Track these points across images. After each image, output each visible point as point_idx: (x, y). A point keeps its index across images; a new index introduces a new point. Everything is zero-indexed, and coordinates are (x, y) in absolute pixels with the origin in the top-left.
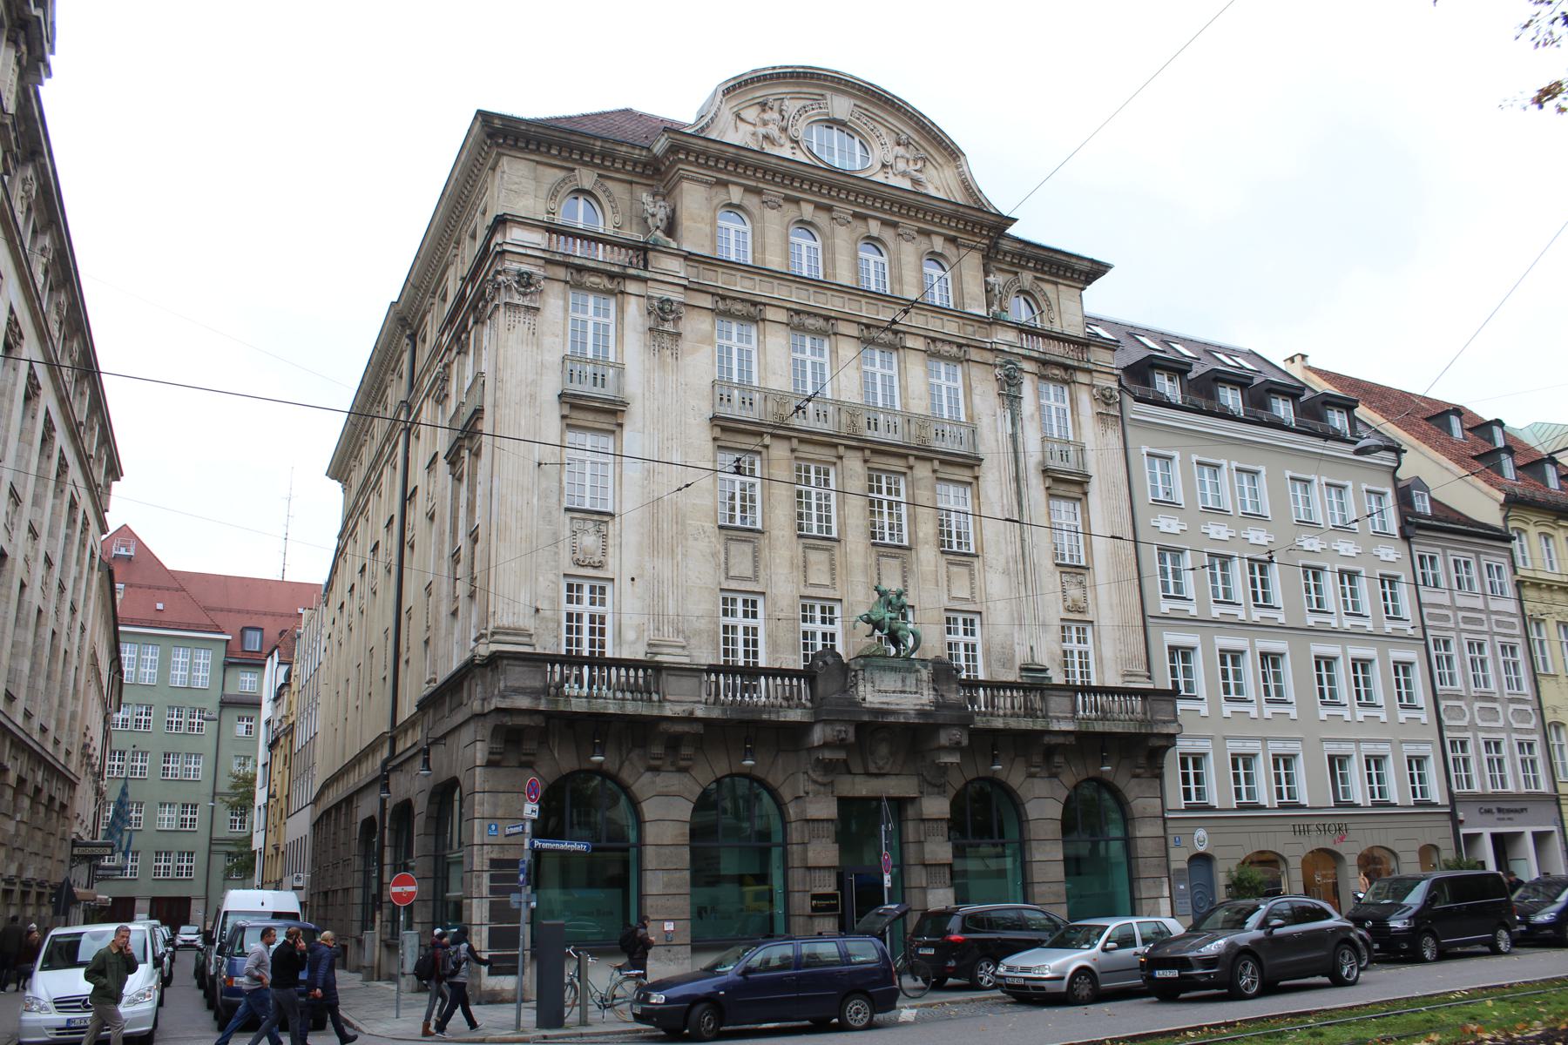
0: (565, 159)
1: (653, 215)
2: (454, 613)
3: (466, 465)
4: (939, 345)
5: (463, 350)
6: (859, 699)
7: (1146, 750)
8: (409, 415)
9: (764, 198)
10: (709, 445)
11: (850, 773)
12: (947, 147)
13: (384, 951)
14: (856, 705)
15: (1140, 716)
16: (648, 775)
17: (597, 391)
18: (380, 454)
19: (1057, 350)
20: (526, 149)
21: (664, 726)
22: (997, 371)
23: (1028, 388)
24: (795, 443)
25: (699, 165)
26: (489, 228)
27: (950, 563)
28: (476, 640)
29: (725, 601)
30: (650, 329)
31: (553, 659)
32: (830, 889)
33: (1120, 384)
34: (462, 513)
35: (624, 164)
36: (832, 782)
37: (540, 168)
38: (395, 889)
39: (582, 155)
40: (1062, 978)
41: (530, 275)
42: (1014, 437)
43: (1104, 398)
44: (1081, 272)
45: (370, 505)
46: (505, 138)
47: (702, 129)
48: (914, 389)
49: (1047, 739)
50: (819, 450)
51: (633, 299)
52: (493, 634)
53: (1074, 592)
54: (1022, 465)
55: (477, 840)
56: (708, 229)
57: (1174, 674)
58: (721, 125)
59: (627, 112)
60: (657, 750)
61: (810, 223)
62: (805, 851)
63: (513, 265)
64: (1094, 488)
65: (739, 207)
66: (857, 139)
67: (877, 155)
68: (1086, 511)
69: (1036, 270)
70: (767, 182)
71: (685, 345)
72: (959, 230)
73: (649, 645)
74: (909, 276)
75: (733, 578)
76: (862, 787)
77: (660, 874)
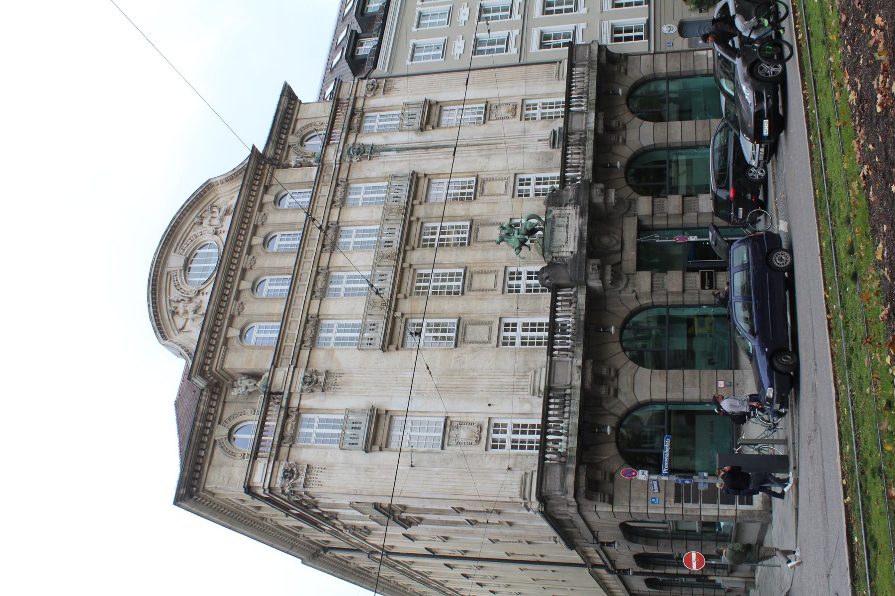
0: (208, 447)
1: (247, 388)
2: (510, 524)
3: (412, 515)
4: (336, 199)
5: (335, 516)
7: (609, 65)
8: (377, 553)
9: (236, 313)
10: (401, 353)
11: (620, 263)
12: (204, 191)
13: (734, 574)
14: (575, 258)
15: (586, 69)
16: (620, 396)
17: (364, 427)
18: (403, 572)
19: (341, 120)
20: (200, 472)
22: (354, 160)
23: (366, 140)
25: (214, 356)
28: (528, 510)
29: (505, 344)
31: (542, 459)
34: (443, 518)
35: (212, 407)
36: (627, 275)
37: (213, 463)
38: (694, 566)
39: (205, 435)
41: (285, 471)
42: (399, 150)
44: (289, 103)
46: (193, 486)
47: (189, 354)
48: (366, 216)
49: (601, 131)
51: (303, 402)
52: (524, 498)
53: (503, 111)
54: (417, 145)
55: (662, 511)
56: (257, 352)
59: (177, 404)
60: (603, 390)
62: (673, 293)
63: (278, 482)
64: (433, 97)
65: (242, 330)
66: (198, 251)
67: (208, 238)
68: (448, 103)
69: (287, 134)
70: (226, 312)
71: (333, 368)
72: (260, 184)
73: (533, 395)
74: (290, 218)
76: (630, 255)
77: (686, 390)
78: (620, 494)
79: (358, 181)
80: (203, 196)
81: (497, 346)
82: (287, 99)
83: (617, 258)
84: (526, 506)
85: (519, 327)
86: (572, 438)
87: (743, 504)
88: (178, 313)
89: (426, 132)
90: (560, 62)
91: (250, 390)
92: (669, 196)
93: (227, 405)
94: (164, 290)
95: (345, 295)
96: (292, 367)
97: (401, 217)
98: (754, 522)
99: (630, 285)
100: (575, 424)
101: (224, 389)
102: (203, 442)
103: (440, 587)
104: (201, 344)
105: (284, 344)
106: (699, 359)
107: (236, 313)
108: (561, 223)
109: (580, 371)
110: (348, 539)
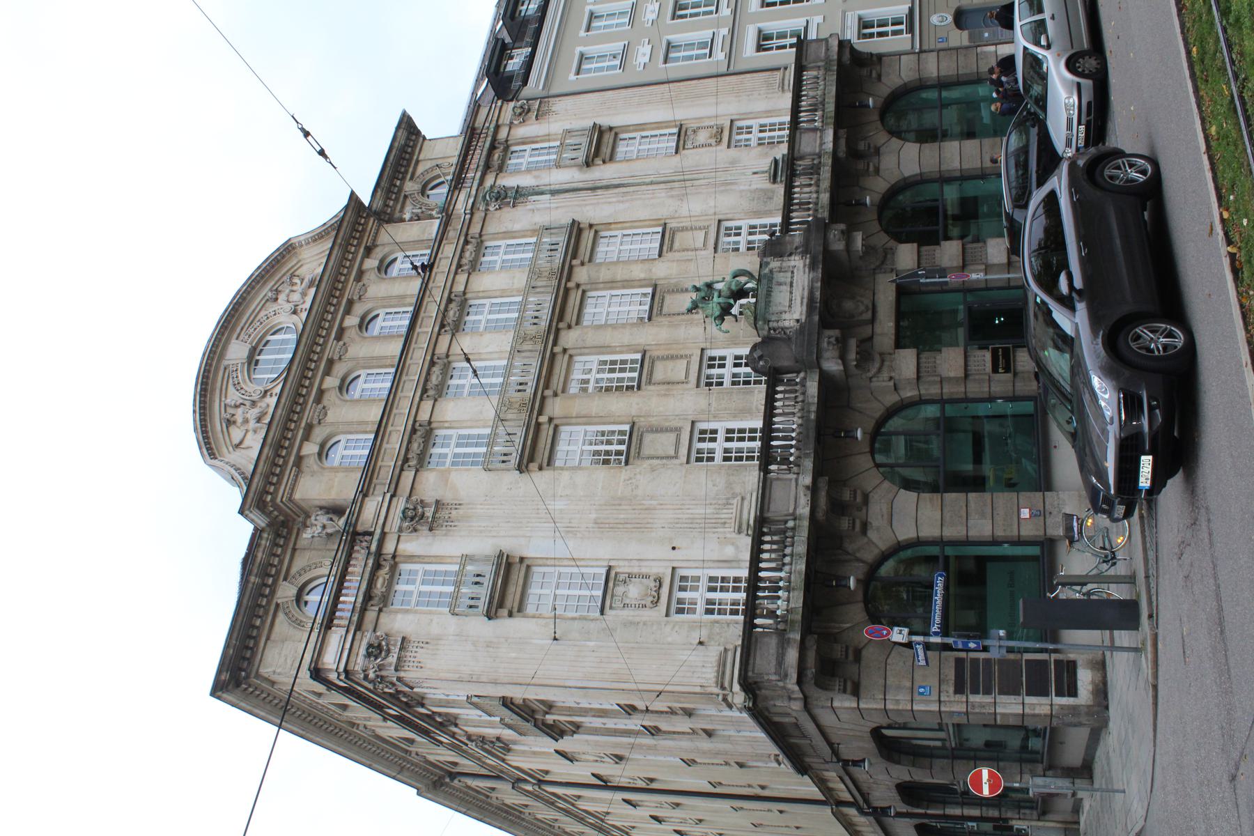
0: (266, 613)
1: (324, 527)
2: (709, 734)
3: (562, 718)
4: (464, 261)
5: (453, 720)
6: (797, 326)
7: (854, 68)
8: (525, 781)
9: (315, 422)
10: (547, 474)
11: (871, 338)
13: (1047, 817)
14: (803, 328)
15: (822, 72)
17: (487, 582)
18: (567, 812)
19: (478, 157)
20: (253, 650)
21: (820, 515)
23: (508, 181)
24: (548, 393)
25: (279, 483)
26: (329, 689)
27: (671, 249)
28: (730, 706)
29: (699, 460)
30: (431, 529)
31: (749, 626)
32: (988, 356)
33: (512, 100)
34: (610, 723)
35: (275, 555)
36: (881, 354)
37: (273, 636)
38: (985, 773)
39: (263, 596)
40: (1079, 85)
41: (370, 646)
42: (554, 193)
43: (523, 113)
44: (408, 139)
45: (618, 824)
46: (241, 670)
47: (244, 478)
48: (505, 285)
49: (842, 154)
50: (556, 370)
51: (401, 546)
52: (723, 688)
54: (581, 185)
55: (935, 707)
56: (340, 475)
57: (784, 47)
58: (244, 462)
59: (247, 562)
60: (845, 524)
61: (343, 380)
62: (949, 379)
63: (359, 662)
64: (605, 121)
65: (322, 446)
66: (269, 338)
67: (285, 319)
68: (626, 128)
69: (403, 179)
70: (300, 419)
71: (448, 497)
72: (359, 245)
73: (739, 532)
74: (397, 289)
75: (677, 451)
76: (886, 325)
77: (971, 522)
78: (871, 680)
79: (497, 236)
80: (279, 262)
81: (688, 462)
82: (405, 134)
83: (866, 331)
84: (725, 700)
85: (721, 436)
86: (796, 593)
87: (1063, 695)
88: (234, 422)
89: (593, 168)
90: (786, 68)
91: (329, 531)
92: (943, 243)
93: (297, 553)
94: (218, 391)
95: (470, 394)
96: (388, 495)
97: (555, 282)
98: (1080, 724)
99: (885, 369)
100: (800, 573)
101: (295, 531)
102: (260, 606)
103: (599, 822)
104: (261, 463)
105: (379, 463)
106: (991, 482)
107: (315, 422)
108: (783, 280)
109: (809, 493)
110: (479, 759)
